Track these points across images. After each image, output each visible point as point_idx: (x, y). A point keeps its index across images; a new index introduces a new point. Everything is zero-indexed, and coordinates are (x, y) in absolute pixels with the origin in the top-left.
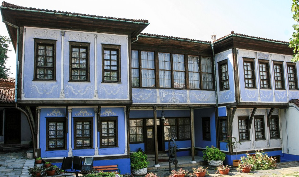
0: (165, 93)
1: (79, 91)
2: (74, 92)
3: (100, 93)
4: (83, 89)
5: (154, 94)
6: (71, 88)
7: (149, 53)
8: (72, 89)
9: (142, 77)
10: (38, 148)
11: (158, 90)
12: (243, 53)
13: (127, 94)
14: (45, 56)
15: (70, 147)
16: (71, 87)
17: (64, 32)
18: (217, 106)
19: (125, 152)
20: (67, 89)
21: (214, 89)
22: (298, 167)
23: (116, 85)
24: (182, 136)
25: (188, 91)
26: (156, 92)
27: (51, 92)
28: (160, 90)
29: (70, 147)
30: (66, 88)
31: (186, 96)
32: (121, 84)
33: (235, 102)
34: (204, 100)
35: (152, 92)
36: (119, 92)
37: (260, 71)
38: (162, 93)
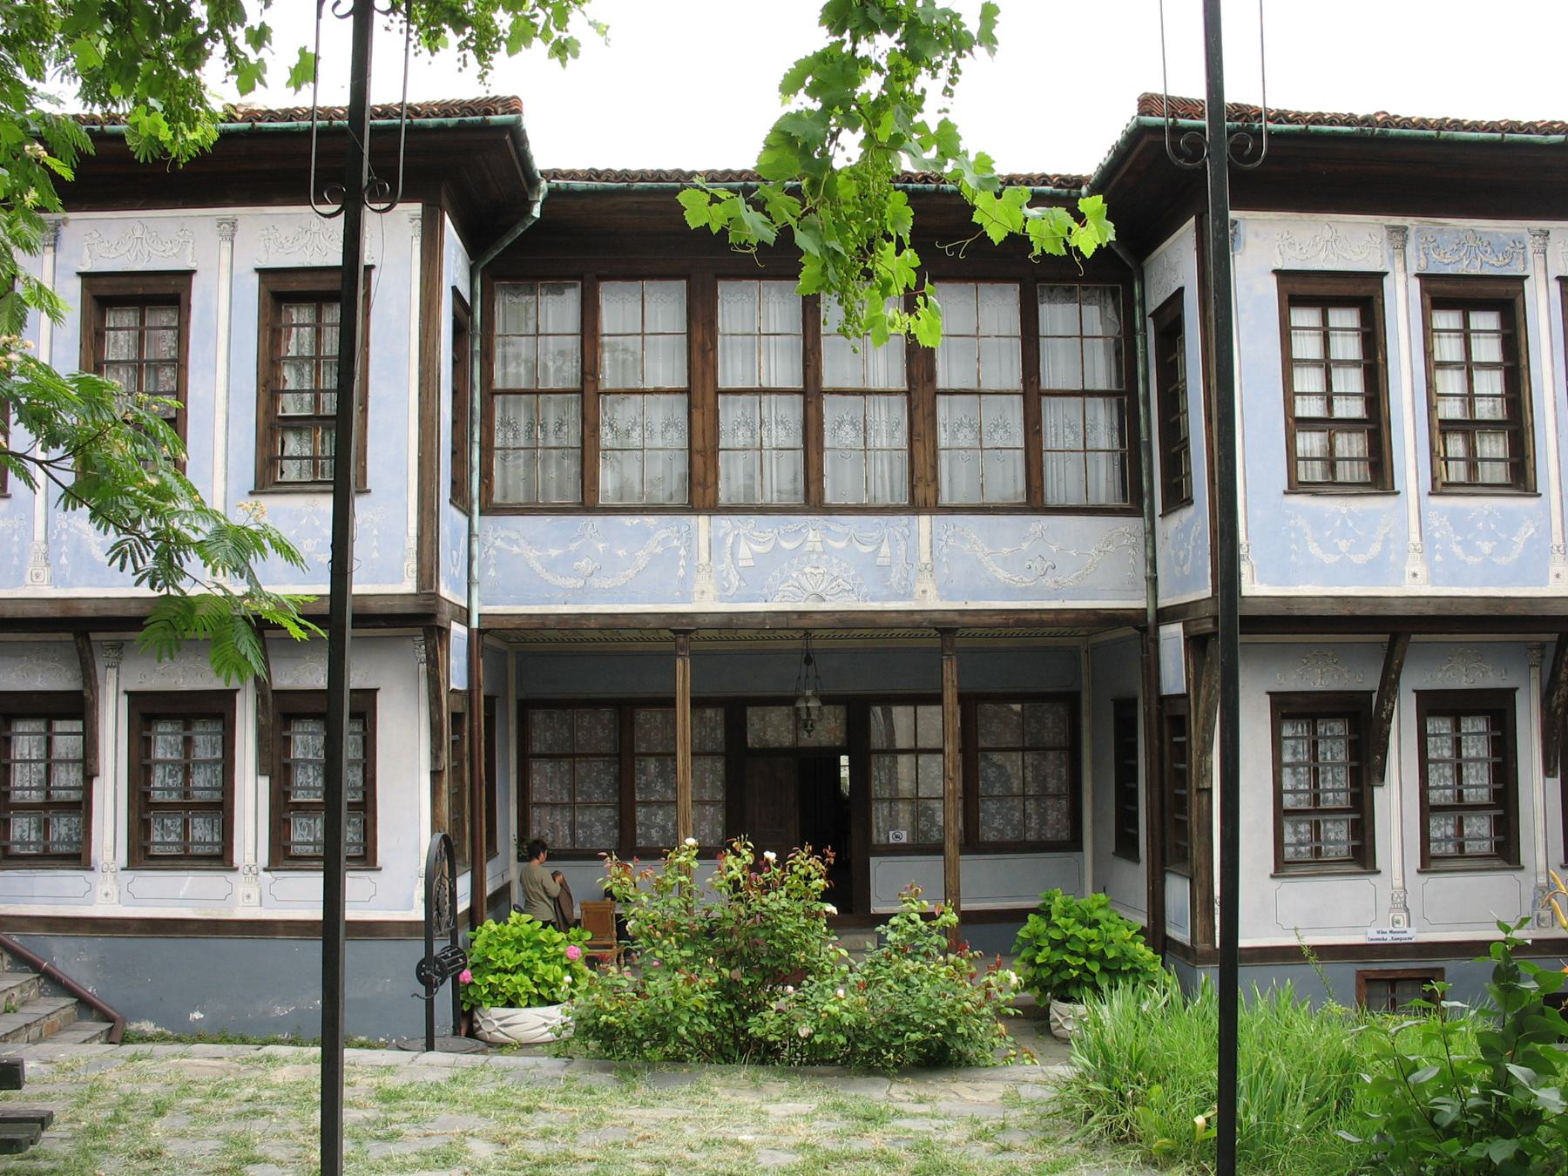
5: (678, 548)
6: (80, 530)
7: (651, 287)
9: (827, 444)
11: (703, 520)
12: (1268, 245)
13: (404, 558)
20: (64, 537)
21: (1132, 501)
22: (319, 1049)
24: (1009, 822)
26: (690, 541)
28: (716, 519)
34: (1048, 582)
35: (663, 534)
37: (1433, 365)
38: (730, 541)
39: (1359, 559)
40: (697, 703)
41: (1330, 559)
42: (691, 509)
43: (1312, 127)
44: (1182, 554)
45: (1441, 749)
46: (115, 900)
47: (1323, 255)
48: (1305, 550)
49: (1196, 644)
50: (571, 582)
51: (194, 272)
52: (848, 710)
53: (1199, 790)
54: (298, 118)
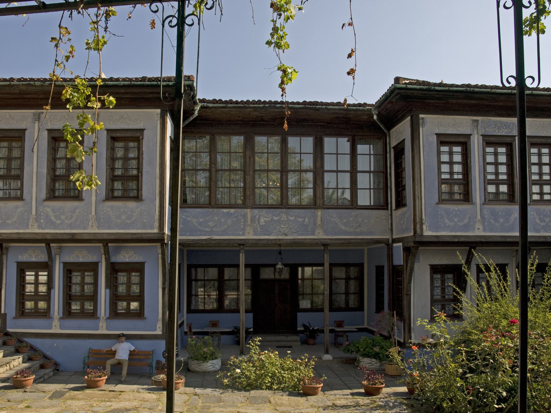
0: (304, 216)
1: (63, 217)
2: (53, 219)
3: (102, 220)
4: (70, 214)
8: (51, 213)
10: (3, 312)
12: (433, 124)
14: (126, 159)
15: (56, 314)
16: (49, 210)
17: (39, 114)
18: (390, 242)
19: (158, 328)
20: (42, 214)
21: (383, 205)
23: (132, 204)
25: (319, 213)
27: (14, 220)
29: (56, 314)
30: (40, 213)
31: (315, 223)
32: (141, 202)
33: (412, 234)
34: (358, 230)
36: (143, 216)
38: (257, 217)
39: (461, 224)
40: (246, 266)
41: (451, 224)
42: (244, 206)
43: (451, 88)
44: (402, 222)
45: (438, 283)
46: (58, 328)
47: (451, 129)
48: (443, 221)
49: (407, 250)
50: (207, 229)
51: (144, 129)
52: (290, 270)
53: (407, 295)
54: (153, 81)
